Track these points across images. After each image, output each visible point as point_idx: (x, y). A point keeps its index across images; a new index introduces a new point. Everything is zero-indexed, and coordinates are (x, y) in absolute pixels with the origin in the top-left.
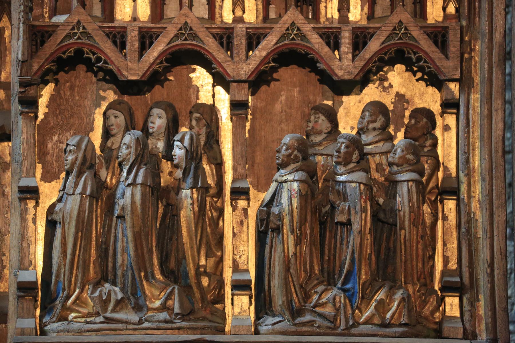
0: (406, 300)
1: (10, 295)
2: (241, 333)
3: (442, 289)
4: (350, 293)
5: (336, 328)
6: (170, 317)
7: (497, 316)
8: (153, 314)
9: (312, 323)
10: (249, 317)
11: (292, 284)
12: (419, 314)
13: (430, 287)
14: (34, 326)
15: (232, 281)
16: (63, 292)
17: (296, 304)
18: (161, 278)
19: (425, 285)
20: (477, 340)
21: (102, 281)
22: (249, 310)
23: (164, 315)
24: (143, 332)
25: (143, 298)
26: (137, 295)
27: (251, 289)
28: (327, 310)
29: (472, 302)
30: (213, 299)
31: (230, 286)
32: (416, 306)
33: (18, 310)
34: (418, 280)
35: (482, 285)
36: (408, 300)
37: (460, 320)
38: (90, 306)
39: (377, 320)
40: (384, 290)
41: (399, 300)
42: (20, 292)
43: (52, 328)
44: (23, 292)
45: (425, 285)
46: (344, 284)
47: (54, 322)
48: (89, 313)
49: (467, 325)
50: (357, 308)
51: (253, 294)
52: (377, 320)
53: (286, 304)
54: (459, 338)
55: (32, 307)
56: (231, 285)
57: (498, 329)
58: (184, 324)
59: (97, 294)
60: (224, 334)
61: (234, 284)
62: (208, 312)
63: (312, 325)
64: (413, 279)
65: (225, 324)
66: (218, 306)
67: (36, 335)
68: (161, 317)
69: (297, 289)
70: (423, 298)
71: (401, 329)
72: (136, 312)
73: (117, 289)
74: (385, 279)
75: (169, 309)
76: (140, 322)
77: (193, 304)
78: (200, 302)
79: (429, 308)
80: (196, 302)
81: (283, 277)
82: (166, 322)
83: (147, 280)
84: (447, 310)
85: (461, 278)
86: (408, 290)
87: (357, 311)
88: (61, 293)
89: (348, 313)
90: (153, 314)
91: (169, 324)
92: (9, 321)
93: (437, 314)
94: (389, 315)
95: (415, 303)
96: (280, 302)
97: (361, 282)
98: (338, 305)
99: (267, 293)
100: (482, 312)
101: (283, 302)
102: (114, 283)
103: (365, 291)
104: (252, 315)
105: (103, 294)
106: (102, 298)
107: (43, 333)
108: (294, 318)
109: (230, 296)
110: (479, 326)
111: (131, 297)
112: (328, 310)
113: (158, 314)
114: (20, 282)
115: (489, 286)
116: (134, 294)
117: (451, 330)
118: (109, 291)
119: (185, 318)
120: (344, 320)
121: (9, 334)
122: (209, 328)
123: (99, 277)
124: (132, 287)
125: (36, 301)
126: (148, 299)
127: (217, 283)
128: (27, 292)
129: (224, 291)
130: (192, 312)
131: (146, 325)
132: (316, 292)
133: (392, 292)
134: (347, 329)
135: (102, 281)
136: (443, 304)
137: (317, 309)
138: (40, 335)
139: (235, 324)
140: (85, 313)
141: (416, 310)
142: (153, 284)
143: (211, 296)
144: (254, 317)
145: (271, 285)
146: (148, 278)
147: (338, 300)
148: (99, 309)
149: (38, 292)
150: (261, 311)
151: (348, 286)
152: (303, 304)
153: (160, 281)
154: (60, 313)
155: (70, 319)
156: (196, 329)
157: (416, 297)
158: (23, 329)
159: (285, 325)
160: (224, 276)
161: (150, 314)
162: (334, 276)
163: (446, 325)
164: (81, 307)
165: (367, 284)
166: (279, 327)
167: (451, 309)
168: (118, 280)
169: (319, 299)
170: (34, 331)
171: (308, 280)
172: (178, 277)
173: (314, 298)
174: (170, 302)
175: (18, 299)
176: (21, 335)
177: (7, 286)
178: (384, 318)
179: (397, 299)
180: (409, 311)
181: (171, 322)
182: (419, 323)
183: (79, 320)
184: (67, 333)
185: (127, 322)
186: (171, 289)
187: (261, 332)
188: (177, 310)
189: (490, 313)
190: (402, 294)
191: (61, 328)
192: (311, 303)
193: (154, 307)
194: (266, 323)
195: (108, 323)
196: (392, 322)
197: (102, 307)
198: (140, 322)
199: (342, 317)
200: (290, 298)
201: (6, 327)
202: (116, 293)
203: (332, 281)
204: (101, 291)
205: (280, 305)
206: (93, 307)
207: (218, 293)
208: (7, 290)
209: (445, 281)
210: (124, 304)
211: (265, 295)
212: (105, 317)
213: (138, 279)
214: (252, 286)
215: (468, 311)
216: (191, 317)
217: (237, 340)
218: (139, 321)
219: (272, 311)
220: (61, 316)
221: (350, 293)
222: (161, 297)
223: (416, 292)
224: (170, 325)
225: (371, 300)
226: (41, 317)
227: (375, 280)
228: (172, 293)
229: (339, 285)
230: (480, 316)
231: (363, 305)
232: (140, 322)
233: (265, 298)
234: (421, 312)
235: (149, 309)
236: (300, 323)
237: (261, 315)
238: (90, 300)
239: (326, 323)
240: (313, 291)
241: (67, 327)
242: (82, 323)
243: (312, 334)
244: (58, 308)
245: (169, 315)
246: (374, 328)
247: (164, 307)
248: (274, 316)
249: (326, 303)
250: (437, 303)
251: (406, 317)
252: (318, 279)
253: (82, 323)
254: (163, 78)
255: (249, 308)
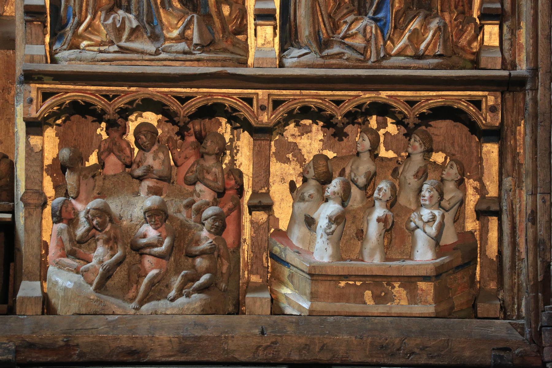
0: (442, 29)
1: (17, 19)
2: (265, 65)
3: (481, 17)
4: (382, 23)
5: (366, 60)
6: (189, 47)
7: (539, 44)
8: (170, 44)
9: (340, 55)
10: (273, 49)
11: (319, 14)
12: (455, 45)
13: (468, 15)
14: (43, 53)
15: (255, 10)
16: (74, 18)
17: (324, 35)
18: (179, 6)
19: (463, 13)
20: (516, 70)
21: (115, 7)
22: (274, 42)
23: (182, 46)
24: (160, 63)
25: (159, 27)
26: (153, 23)
27: (275, 19)
28: (357, 41)
29: (512, 30)
30: (235, 29)
31: (253, 16)
32: (452, 36)
33: (26, 36)
34: (456, 8)
35: (525, 12)
36: (444, 30)
37: (499, 49)
38: (103, 35)
39: (410, 52)
40: (418, 19)
41: (434, 29)
42: (27, 16)
43: (63, 56)
44: (30, 16)
45: (463, 13)
46: (375, 13)
47: (65, 50)
48: (102, 41)
49: (507, 55)
50: (390, 39)
51: (278, 25)
52: (410, 52)
53: (312, 35)
54: (497, 68)
55: (41, 33)
56: (254, 15)
57: (540, 57)
58: (204, 55)
59: (110, 21)
60: (247, 67)
61: (258, 13)
62: (229, 43)
63: (341, 58)
64: (450, 6)
65: (247, 56)
66: (240, 37)
67: (47, 62)
68: (179, 48)
69: (325, 19)
70: (461, 27)
71: (436, 61)
72: (152, 42)
73: (131, 16)
74: (420, 7)
75: (187, 39)
76: (157, 53)
77: (213, 34)
78: (220, 32)
79: (466, 37)
80: (216, 33)
81: (310, 6)
82: (185, 53)
83: (164, 8)
84: (485, 39)
85: (502, 5)
86: (444, 19)
87: (389, 42)
88: (71, 18)
89: (379, 45)
90: (170, 44)
91: (188, 56)
92: (17, 47)
93: (475, 44)
94: (423, 46)
95: (452, 32)
96: (307, 33)
97: (394, 10)
98: (368, 36)
99: (293, 24)
100: (523, 40)
101: (310, 33)
102: (128, 10)
103: (398, 20)
104: (277, 47)
105: (117, 22)
106: (116, 26)
107: (54, 61)
108: (321, 50)
109: (253, 27)
110: (519, 55)
111: (147, 26)
112: (358, 42)
113: (176, 44)
114: (27, 5)
115: (532, 12)
116: (150, 22)
117: (489, 60)
118: (123, 19)
119: (205, 49)
120: (375, 51)
121: (18, 62)
122: (230, 60)
123: (112, 3)
124: (147, 15)
125: (45, 27)
126: (165, 28)
127: (239, 12)
128: (35, 17)
129: (247, 21)
130: (212, 43)
131: (163, 55)
132: (345, 22)
133: (427, 21)
134: (377, 61)
135: (115, 7)
136: (482, 33)
137: (347, 41)
138: (50, 63)
139: (259, 55)
140: (97, 41)
141: (452, 40)
142: (170, 12)
143: (232, 27)
144: (279, 49)
145: (297, 15)
146: (165, 5)
147: (368, 30)
148: (113, 37)
149: (47, 17)
150: (286, 43)
151: (380, 15)
152: (331, 35)
153: (177, 9)
154: (71, 40)
155: (81, 47)
156: (216, 60)
157: (453, 25)
158: (32, 56)
159: (311, 58)
160: (246, 4)
161: (167, 44)
162: (365, 4)
163: (484, 56)
164: (93, 34)
165: (401, 13)
166: (305, 60)
167: (490, 38)
168: (133, 7)
169: (348, 29)
170: (44, 59)
171: (337, 9)
172: (197, 5)
173: (343, 28)
174: (189, 32)
175: (26, 24)
176: (30, 62)
177: (13, 10)
178: (417, 49)
179: (432, 29)
180: (445, 41)
181: (190, 53)
182: (455, 54)
183: (92, 48)
184: (79, 62)
185: (143, 53)
186: (189, 18)
187: (286, 65)
188: (196, 40)
189: (531, 41)
190: (438, 23)
191: (73, 57)
192: (339, 34)
193: (171, 37)
194: (291, 56)
195: (122, 53)
196: (426, 53)
197: (116, 36)
198: (157, 53)
199: (373, 49)
200: (317, 29)
201: (14, 53)
202: (130, 21)
203: (362, 10)
204: (114, 19)
205: (307, 36)
206: (107, 35)
207: (240, 23)
208: (13, 14)
209: (484, 8)
210: (139, 33)
211: (290, 25)
212: (119, 47)
213: (154, 6)
214: (276, 15)
215: (508, 41)
216: (211, 48)
217: (260, 73)
218: (156, 52)
219: (298, 42)
220: (73, 44)
221: (382, 23)
222: (179, 26)
223: (453, 21)
224: (188, 57)
225: (404, 30)
226: (51, 44)
227: (409, 8)
228: (190, 22)
229: (370, 14)
230: (520, 45)
231: (395, 36)
232: (157, 53)
233: (290, 29)
234: (458, 42)
235: (166, 39)
236: (328, 55)
237: (286, 47)
238: (103, 28)
239: (355, 55)
240: (342, 21)
241: (79, 56)
242: (95, 51)
243: (340, 67)
244: (69, 34)
245: (188, 46)
246: (407, 60)
247: (182, 38)
248: (300, 48)
249: (356, 34)
250: (475, 31)
251: (441, 47)
252: (347, 8)
253: (95, 51)
254: (55, 175)
255: (273, 40)
